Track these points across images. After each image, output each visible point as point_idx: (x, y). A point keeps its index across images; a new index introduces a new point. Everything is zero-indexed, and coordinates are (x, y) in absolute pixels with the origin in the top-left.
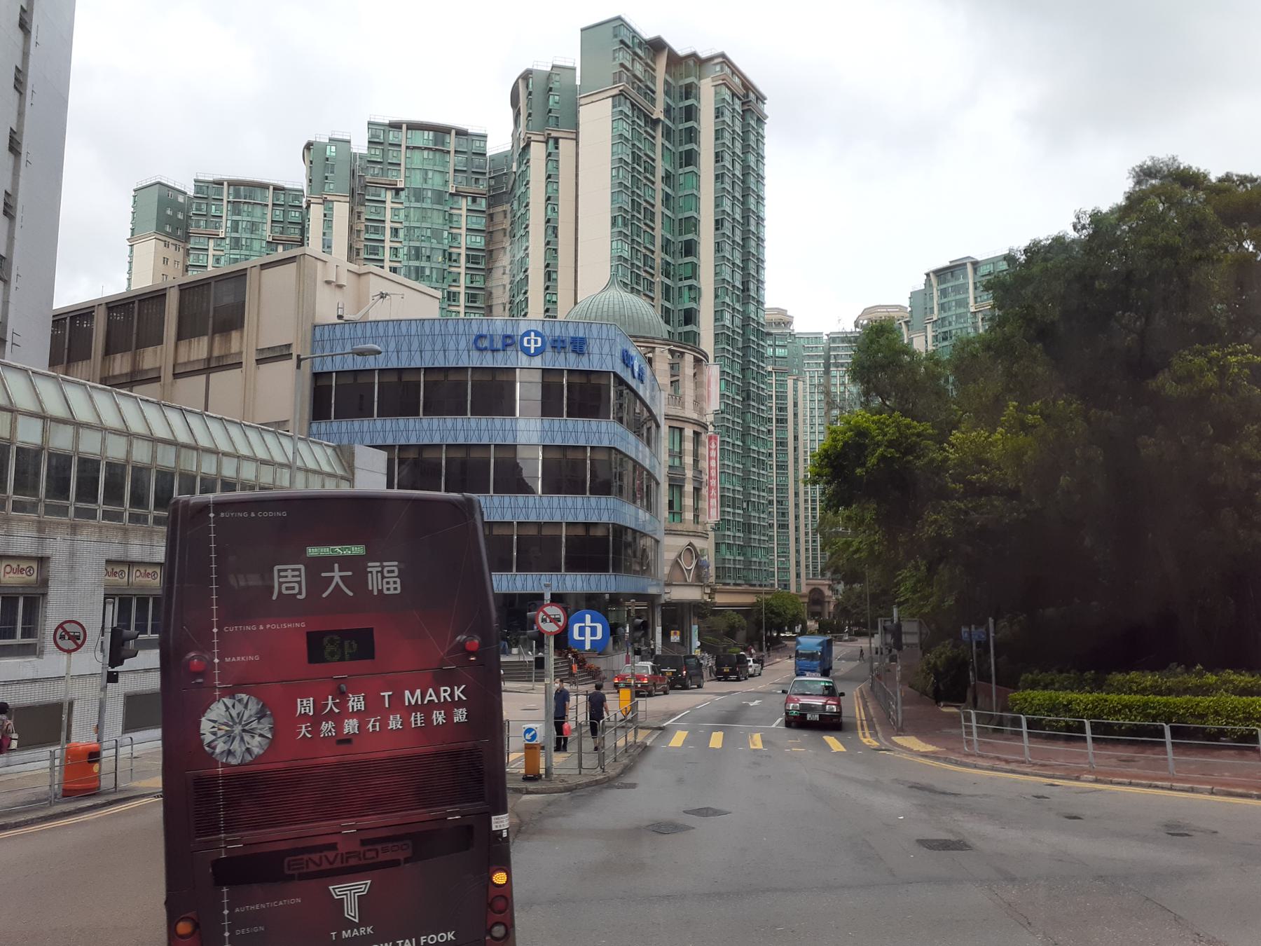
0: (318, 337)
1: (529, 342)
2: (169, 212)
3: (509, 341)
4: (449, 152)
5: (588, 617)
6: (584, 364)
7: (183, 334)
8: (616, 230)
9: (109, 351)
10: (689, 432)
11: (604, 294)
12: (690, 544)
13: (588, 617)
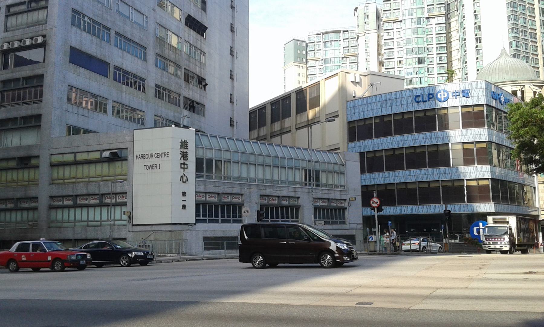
0: (349, 105)
2: (299, 52)
3: (431, 96)
4: (340, 40)
5: (481, 224)
6: (469, 102)
7: (273, 121)
8: (510, 22)
9: (273, 121)
11: (499, 60)
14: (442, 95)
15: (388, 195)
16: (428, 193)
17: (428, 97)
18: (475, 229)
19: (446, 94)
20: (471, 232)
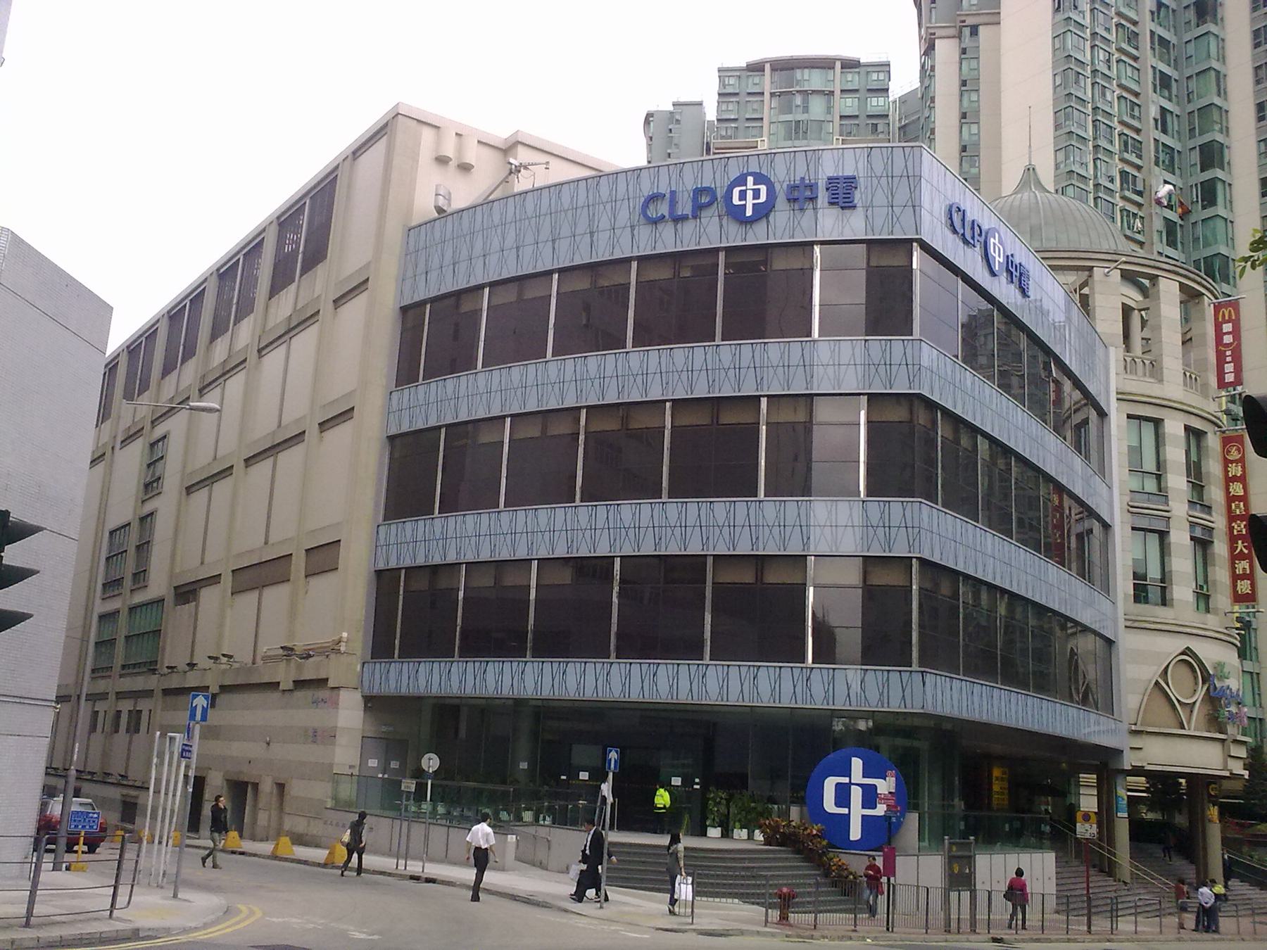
1: (743, 195)
5: (857, 764)
10: (1174, 427)
12: (1187, 651)
13: (857, 764)
14: (750, 194)
15: (490, 614)
16: (662, 605)
17: (695, 199)
18: (830, 784)
19: (763, 188)
20: (807, 794)
